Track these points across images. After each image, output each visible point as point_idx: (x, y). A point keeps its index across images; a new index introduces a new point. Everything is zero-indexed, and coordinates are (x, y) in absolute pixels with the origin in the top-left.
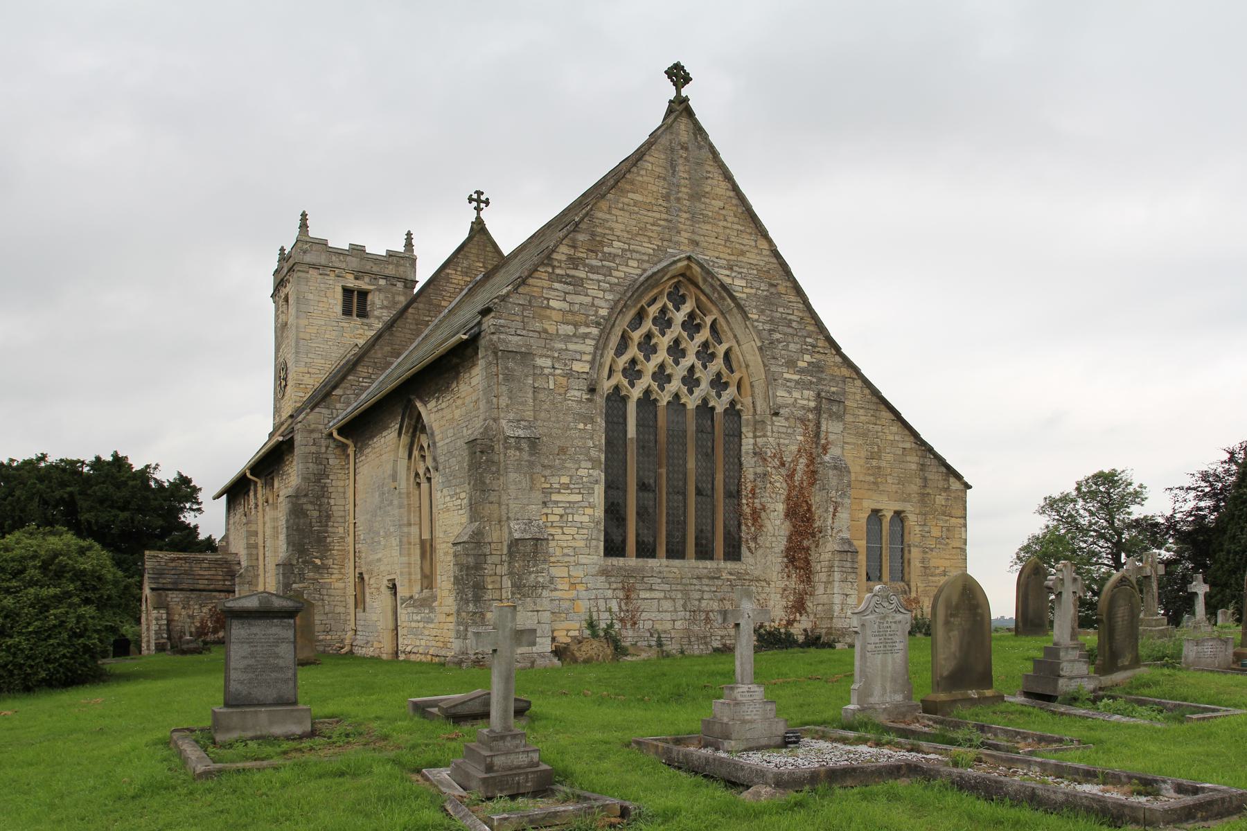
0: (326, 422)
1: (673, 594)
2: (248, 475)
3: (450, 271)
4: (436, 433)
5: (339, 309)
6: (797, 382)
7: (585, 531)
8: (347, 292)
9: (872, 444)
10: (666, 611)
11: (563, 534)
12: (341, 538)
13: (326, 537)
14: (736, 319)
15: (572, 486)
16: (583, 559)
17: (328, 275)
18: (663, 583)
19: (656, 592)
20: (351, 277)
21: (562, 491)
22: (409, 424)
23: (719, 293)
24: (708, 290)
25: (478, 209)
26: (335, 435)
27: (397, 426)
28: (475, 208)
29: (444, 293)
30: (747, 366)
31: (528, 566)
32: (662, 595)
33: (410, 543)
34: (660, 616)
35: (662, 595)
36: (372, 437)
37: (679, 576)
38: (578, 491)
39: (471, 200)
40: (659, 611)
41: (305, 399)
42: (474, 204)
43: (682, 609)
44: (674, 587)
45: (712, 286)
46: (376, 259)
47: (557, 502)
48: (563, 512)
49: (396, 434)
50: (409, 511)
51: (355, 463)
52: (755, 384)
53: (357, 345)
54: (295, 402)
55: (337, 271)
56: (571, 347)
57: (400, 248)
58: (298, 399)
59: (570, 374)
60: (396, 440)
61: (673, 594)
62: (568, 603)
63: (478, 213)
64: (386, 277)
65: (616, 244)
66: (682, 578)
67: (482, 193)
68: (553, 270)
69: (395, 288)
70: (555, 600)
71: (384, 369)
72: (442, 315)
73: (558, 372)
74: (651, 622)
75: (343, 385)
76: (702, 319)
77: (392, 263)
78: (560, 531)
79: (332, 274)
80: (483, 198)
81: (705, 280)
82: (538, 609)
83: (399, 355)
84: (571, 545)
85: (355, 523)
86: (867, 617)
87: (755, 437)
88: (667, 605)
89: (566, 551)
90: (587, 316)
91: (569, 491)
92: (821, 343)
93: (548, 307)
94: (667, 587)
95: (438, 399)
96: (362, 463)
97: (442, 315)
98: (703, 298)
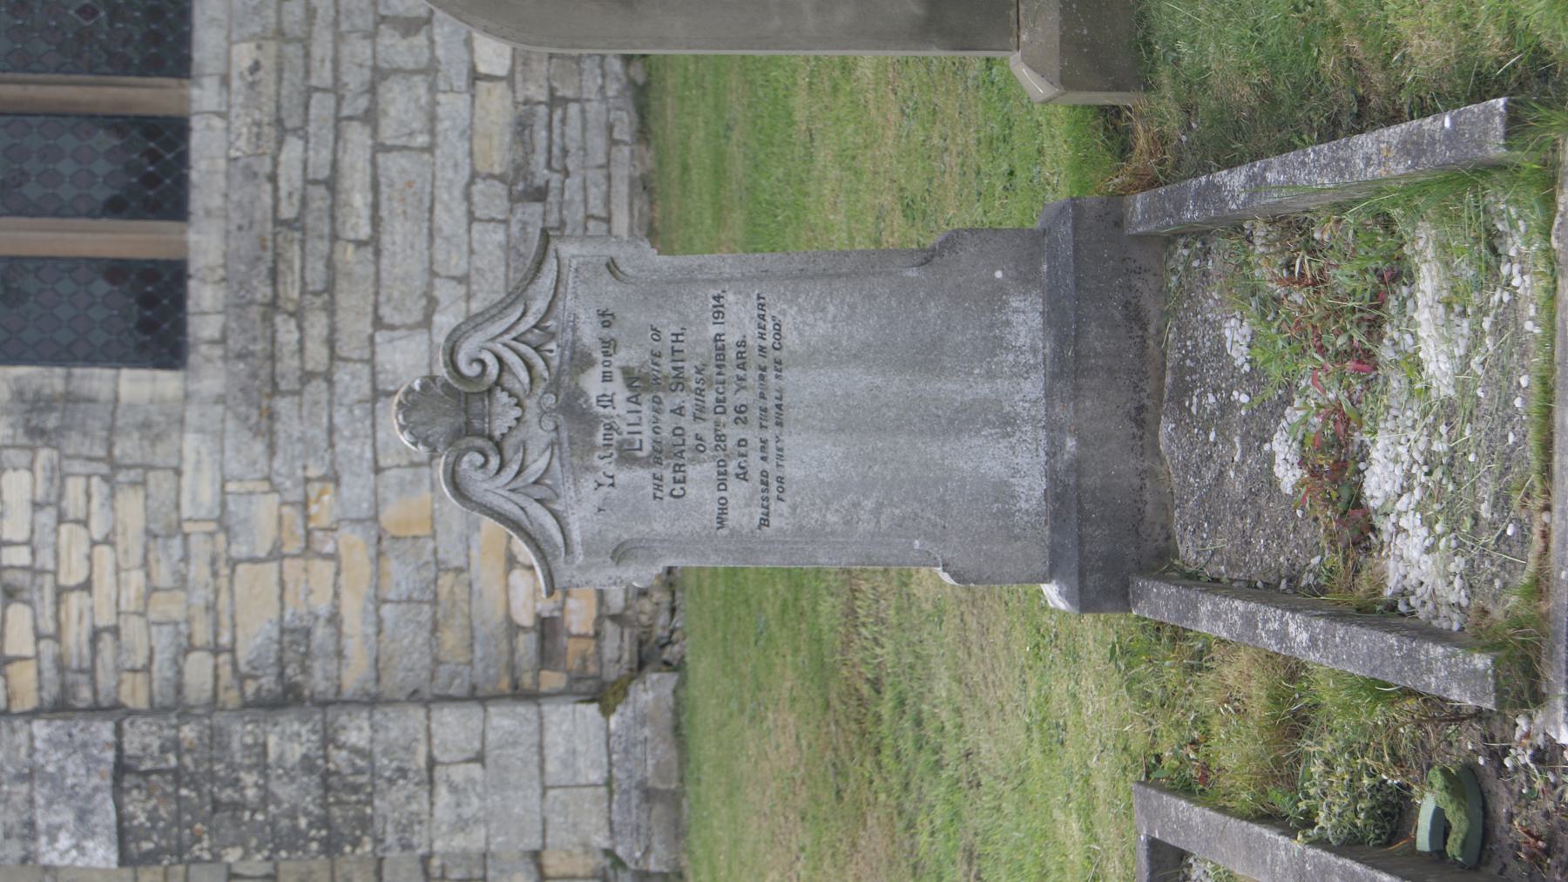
1: (355, 79)
7: (75, 487)
10: (433, 119)
11: (87, 586)
16: (199, 493)
18: (302, 132)
19: (346, 160)
31: (237, 806)
32: (358, 136)
34: (452, 147)
37: (271, 48)
40: (430, 149)
43: (420, 40)
44: (322, 76)
61: (355, 79)
62: (392, 566)
66: (280, 34)
70: (379, 623)
74: (480, 186)
78: (75, 601)
82: (421, 760)
84: (136, 556)
86: (576, 536)
88: (400, 103)
89: (163, 576)
94: (322, 107)
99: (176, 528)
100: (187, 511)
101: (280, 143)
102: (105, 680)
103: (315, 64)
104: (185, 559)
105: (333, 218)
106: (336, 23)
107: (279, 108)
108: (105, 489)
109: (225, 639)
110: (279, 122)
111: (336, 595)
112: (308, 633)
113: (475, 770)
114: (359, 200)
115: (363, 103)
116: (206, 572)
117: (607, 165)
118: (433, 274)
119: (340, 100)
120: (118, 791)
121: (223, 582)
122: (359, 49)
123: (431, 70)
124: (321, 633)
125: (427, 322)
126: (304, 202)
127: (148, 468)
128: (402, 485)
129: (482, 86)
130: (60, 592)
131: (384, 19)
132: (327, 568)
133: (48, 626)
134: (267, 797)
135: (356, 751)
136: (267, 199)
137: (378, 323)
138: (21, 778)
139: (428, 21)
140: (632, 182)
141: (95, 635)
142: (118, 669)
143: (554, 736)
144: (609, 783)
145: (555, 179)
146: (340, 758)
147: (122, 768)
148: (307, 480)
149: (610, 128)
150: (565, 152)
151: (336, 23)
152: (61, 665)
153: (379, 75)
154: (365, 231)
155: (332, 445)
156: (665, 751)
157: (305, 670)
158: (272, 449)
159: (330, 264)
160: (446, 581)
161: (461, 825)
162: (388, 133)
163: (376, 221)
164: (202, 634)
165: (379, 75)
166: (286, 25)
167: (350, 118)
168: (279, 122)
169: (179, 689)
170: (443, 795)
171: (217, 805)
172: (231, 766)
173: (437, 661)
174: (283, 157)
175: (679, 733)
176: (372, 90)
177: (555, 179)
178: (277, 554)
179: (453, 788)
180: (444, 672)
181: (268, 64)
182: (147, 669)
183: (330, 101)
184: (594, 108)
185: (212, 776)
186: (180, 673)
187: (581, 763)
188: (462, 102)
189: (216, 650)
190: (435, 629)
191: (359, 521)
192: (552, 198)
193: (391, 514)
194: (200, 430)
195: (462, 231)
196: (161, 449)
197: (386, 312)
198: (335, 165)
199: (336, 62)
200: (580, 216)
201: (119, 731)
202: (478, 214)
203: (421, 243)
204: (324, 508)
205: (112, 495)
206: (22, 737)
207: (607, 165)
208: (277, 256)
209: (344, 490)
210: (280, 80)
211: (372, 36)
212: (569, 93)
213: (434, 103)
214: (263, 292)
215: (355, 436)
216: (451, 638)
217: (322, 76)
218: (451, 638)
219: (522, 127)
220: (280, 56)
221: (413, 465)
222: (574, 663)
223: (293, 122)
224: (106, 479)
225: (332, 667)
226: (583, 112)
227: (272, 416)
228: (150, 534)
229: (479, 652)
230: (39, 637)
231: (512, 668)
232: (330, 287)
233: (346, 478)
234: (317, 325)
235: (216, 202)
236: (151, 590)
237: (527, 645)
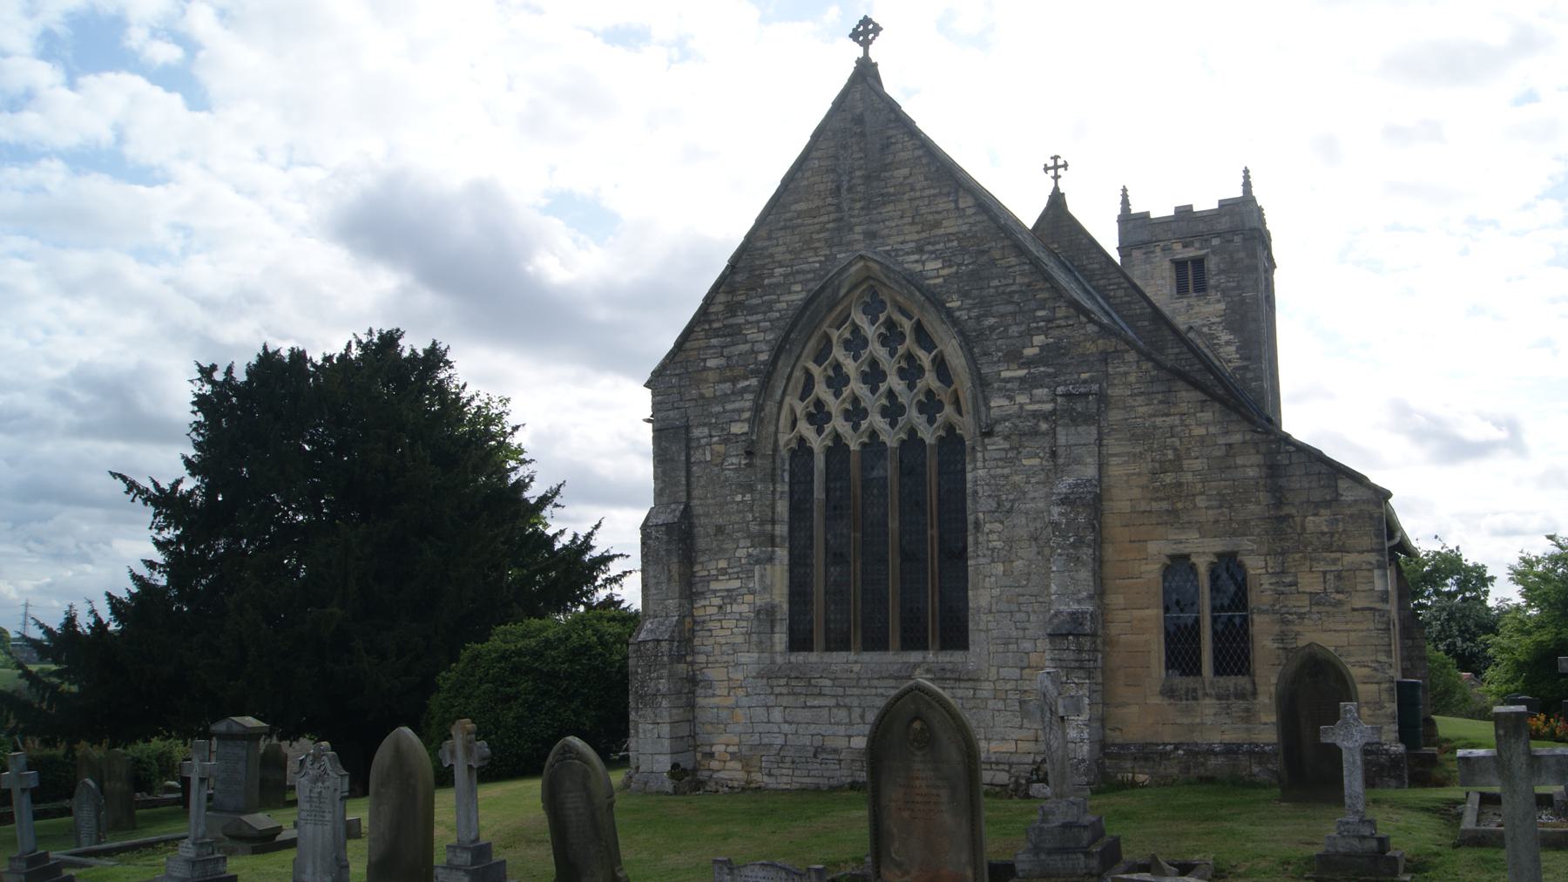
1: (848, 700)
6: (1022, 380)
7: (744, 624)
8: (1180, 265)
10: (838, 724)
11: (722, 628)
15: (730, 571)
16: (744, 658)
17: (1153, 252)
18: (833, 686)
19: (826, 698)
20: (1178, 247)
21: (720, 578)
28: (1053, 178)
32: (832, 702)
35: (832, 702)
38: (736, 576)
40: (830, 724)
43: (859, 721)
44: (849, 691)
47: (715, 591)
48: (721, 603)
55: (1162, 244)
56: (729, 407)
57: (1237, 192)
59: (727, 439)
61: (848, 700)
64: (1218, 235)
65: (778, 271)
68: (710, 325)
73: (715, 439)
74: (821, 738)
79: (1158, 249)
82: (659, 721)
88: (841, 714)
89: (724, 648)
90: (746, 366)
91: (727, 577)
93: (705, 369)
94: (840, 691)
99: (735, 652)
100: (739, 654)
101: (830, 679)
102: (700, 633)
103: (851, 689)
104: (728, 654)
105: (811, 695)
106: (862, 695)
107: (840, 679)
108: (744, 632)
109: (710, 665)
110: (836, 679)
111: (720, 696)
112: (711, 688)
113: (656, 736)
114: (816, 703)
115: (842, 703)
116: (724, 660)
117: (823, 776)
118: (798, 724)
119: (841, 696)
120: (653, 640)
121: (722, 665)
122: (856, 703)
123: (851, 724)
124: (711, 691)
125: (786, 722)
126: (816, 686)
127: (749, 643)
128: (745, 714)
129: (847, 739)
130: (720, 620)
131: (864, 709)
132: (726, 694)
133: (713, 618)
134: (651, 679)
135: (661, 703)
136: (815, 676)
137: (785, 708)
138: (667, 614)
139: (864, 723)
140: (819, 784)
141: (710, 630)
142: (703, 637)
143: (661, 758)
144: (652, 772)
145: (819, 761)
146: (659, 699)
147: (658, 641)
148: (746, 688)
149: (833, 778)
150: (826, 764)
151: (862, 695)
152: (704, 622)
153: (849, 708)
154: (808, 704)
155: (756, 694)
156: (655, 788)
157: (702, 688)
158: (754, 678)
159: (800, 694)
160: (722, 726)
161: (644, 731)
162: (834, 711)
164: (711, 659)
165: (849, 708)
166: (862, 681)
167: (837, 700)
168: (836, 679)
169: (698, 653)
170: (651, 727)
171: (650, 666)
172: (659, 670)
173: (704, 724)
174: (827, 680)
175: (658, 793)
176: (845, 706)
177: (819, 761)
178: (729, 679)
179: (653, 729)
180: (701, 726)
181: (852, 675)
182: (703, 645)
183: (841, 694)
184: (838, 773)
185: (656, 665)
186: (702, 653)
187: (657, 765)
188: (842, 733)
189: (707, 663)
190: (712, 723)
191: (737, 701)
192: (813, 760)
193: (738, 711)
194: (759, 658)
195: (809, 733)
196: (754, 647)
197: (788, 710)
198: (825, 695)
199: (851, 695)
200: (809, 768)
201: (666, 640)
202: (814, 738)
203: (806, 721)
204: (740, 692)
205: (743, 634)
206: (675, 614)
207: (823, 776)
208: (801, 678)
209: (744, 698)
210: (847, 679)
211: (860, 706)
212: (842, 765)
213: (842, 725)
214: (793, 675)
215: (758, 701)
216: (709, 728)
217: (849, 691)
218: (709, 728)
219: (835, 751)
220: (854, 679)
221: (751, 717)
222: (703, 762)
223: (836, 683)
224: (747, 632)
225: (703, 695)
226: (837, 770)
227: (762, 678)
228: (734, 644)
229: (706, 736)
230: (710, 615)
231: (702, 745)
232: (794, 694)
233: (747, 699)
234: (784, 690)
235: (825, 660)
236: (721, 645)
237: (707, 749)
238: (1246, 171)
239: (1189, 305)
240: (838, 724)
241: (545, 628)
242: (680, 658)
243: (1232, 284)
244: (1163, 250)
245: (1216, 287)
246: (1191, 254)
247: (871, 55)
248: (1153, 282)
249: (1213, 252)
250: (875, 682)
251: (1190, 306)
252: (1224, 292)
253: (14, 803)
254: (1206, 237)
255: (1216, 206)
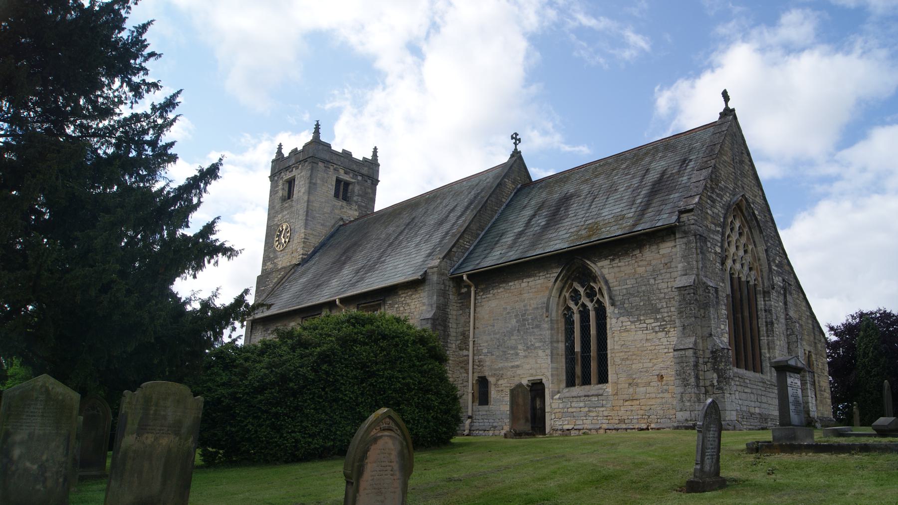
0: (449, 268)
2: (337, 302)
3: (506, 180)
4: (610, 281)
5: (333, 192)
8: (338, 181)
9: (799, 311)
11: (583, 420)
12: (454, 352)
13: (446, 350)
14: (756, 233)
17: (329, 168)
20: (342, 171)
22: (566, 274)
23: (751, 217)
24: (746, 214)
25: (516, 144)
26: (465, 278)
27: (556, 275)
28: (514, 143)
29: (504, 193)
30: (759, 260)
33: (558, 354)
36: (506, 281)
39: (512, 138)
41: (309, 253)
42: (514, 141)
45: (749, 212)
46: (356, 161)
49: (553, 280)
50: (558, 333)
51: (475, 299)
52: (764, 270)
53: (342, 219)
54: (303, 254)
55: (335, 166)
57: (369, 156)
58: (305, 252)
60: (551, 284)
63: (516, 147)
64: (362, 175)
67: (518, 135)
69: (366, 183)
71: (476, 238)
72: (503, 207)
75: (457, 246)
76: (743, 230)
77: (366, 166)
79: (332, 168)
80: (518, 137)
81: (746, 209)
83: (483, 229)
85: (474, 341)
87: (764, 301)
92: (781, 251)
93: (707, 213)
95: (613, 260)
96: (483, 300)
97: (503, 207)
98: (743, 218)
163: (746, 393)
238: (375, 149)
239: (342, 206)
240: (752, 401)
241: (371, 321)
242: (384, 403)
243: (363, 204)
244: (335, 169)
245: (356, 202)
246: (347, 179)
247: (729, 106)
248: (326, 184)
249: (358, 183)
250: (759, 384)
251: (342, 207)
252: (359, 206)
253: (600, 386)
254: (356, 173)
255: (361, 159)
